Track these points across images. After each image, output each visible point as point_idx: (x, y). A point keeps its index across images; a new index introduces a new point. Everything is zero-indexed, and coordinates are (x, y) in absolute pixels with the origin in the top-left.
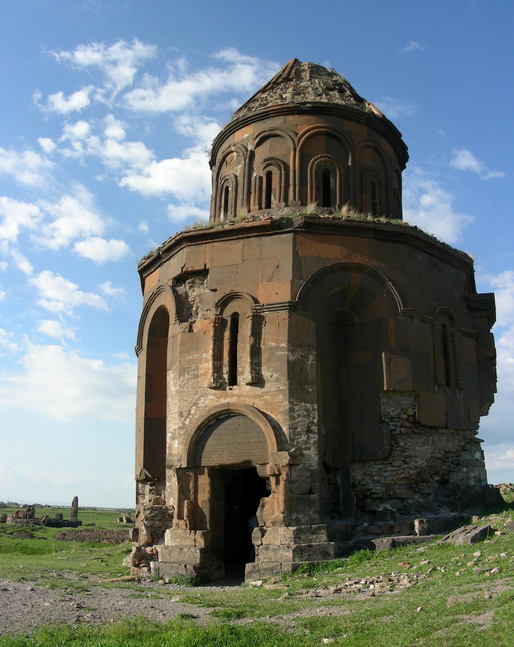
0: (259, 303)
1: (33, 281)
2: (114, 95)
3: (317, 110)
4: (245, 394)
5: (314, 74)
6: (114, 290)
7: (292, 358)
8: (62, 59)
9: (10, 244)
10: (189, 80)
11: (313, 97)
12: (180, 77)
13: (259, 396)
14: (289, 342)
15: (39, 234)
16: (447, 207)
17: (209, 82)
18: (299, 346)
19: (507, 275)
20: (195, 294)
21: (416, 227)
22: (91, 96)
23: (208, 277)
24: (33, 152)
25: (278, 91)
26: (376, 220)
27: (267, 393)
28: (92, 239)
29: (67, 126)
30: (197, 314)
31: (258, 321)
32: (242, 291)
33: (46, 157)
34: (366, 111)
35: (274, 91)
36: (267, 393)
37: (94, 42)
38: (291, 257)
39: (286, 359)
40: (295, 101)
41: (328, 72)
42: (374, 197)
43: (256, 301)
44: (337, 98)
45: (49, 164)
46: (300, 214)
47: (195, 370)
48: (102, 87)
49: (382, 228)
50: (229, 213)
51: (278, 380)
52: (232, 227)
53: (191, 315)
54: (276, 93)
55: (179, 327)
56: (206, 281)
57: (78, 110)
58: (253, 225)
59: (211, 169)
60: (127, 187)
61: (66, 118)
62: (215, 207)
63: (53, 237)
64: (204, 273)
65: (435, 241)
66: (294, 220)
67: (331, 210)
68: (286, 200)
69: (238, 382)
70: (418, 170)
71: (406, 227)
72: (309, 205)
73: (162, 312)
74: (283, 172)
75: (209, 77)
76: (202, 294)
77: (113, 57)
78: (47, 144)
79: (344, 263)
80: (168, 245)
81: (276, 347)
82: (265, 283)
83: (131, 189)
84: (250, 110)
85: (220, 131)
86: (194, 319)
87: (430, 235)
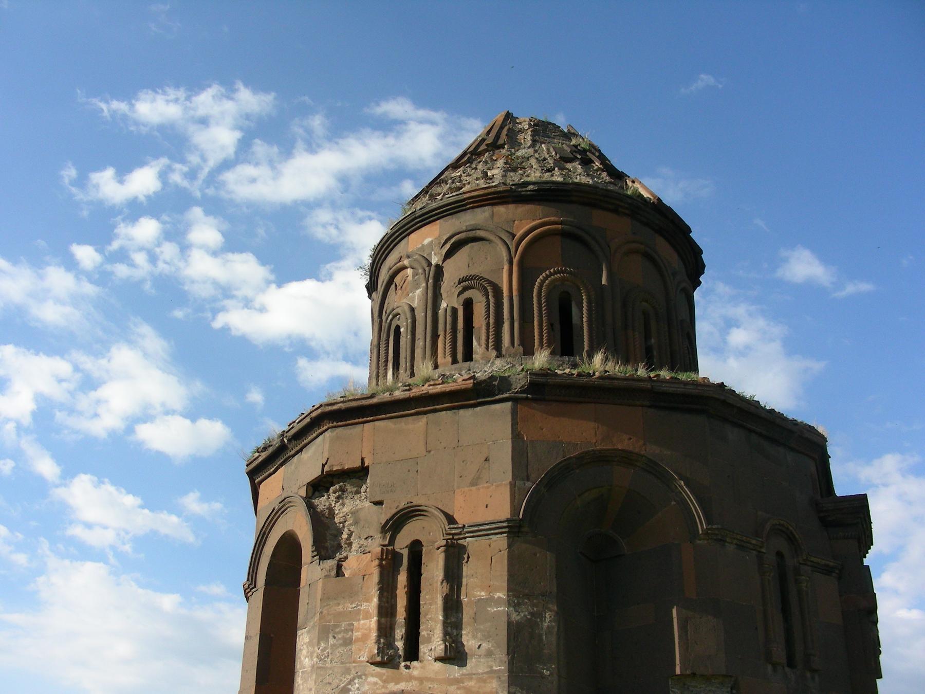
0: (457, 523)
1: (61, 492)
2: (203, 175)
3: (546, 195)
4: (432, 675)
5: (538, 135)
6: (205, 506)
7: (515, 617)
8: (114, 114)
9: (19, 428)
10: (330, 150)
11: (538, 174)
12: (314, 146)
13: (457, 681)
14: (509, 591)
15: (71, 411)
16: (775, 347)
17: (364, 153)
18: (527, 596)
19: (890, 462)
20: (345, 510)
21: (722, 385)
22: (163, 176)
23: (368, 481)
24: (62, 270)
25: (480, 166)
26: (652, 375)
27: (470, 676)
28: (167, 418)
29: (122, 225)
30: (350, 545)
31: (455, 556)
32: (427, 503)
33: (84, 278)
34: (629, 192)
35: (474, 166)
36: (470, 676)
37: (168, 86)
38: (510, 441)
39: (505, 619)
40: (508, 181)
41: (562, 131)
42: (647, 336)
43: (451, 520)
44: (578, 174)
45: (89, 289)
46: (523, 369)
47: (346, 631)
48: (183, 161)
49: (665, 388)
50: (401, 371)
51: (489, 654)
52: (407, 394)
53: (339, 547)
54: (476, 169)
55: (319, 568)
56: (364, 487)
57: (142, 198)
58: (443, 389)
59: (370, 296)
60: (226, 329)
61: (120, 212)
62: (378, 361)
63: (96, 415)
64: (360, 473)
65: (757, 407)
66: (513, 380)
67: (574, 361)
68: (498, 346)
69: (421, 654)
70: (722, 288)
71: (706, 384)
72: (537, 354)
73: (289, 543)
74: (492, 300)
75: (365, 145)
76: (357, 511)
77: (201, 112)
78: (86, 254)
79: (600, 451)
80: (297, 427)
81: (487, 599)
82: (466, 489)
83: (234, 332)
84: (433, 197)
85: (384, 234)
86: (344, 554)
87: (748, 396)
